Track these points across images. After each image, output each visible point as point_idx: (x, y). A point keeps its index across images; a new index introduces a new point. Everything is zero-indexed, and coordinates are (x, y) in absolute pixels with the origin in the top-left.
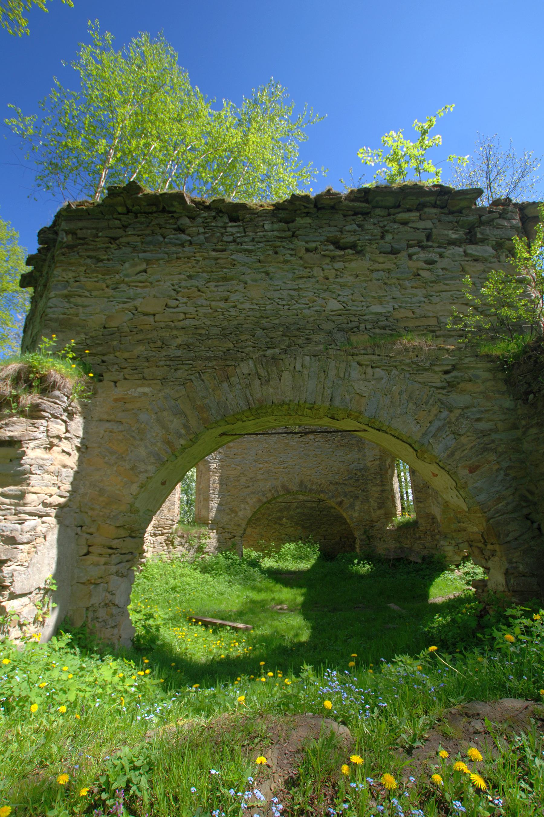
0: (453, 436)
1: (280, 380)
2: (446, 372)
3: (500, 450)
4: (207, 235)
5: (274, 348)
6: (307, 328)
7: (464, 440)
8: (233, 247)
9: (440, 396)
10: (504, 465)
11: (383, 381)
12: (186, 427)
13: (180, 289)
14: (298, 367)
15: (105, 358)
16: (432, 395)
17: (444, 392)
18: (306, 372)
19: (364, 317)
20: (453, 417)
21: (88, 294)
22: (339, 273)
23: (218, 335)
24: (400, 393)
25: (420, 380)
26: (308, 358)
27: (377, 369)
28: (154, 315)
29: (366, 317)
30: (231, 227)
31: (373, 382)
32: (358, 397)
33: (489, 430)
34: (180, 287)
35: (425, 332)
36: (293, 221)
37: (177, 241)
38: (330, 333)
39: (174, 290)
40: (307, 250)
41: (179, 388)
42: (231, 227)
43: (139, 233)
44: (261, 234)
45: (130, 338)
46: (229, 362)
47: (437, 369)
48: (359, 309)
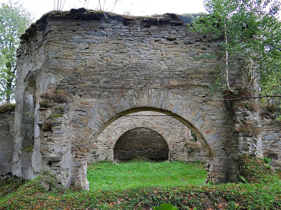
0: (203, 121)
1: (143, 98)
2: (203, 97)
3: (218, 126)
4: (113, 33)
5: (140, 84)
6: (154, 77)
7: (206, 122)
8: (124, 38)
9: (200, 106)
10: (219, 131)
11: (180, 100)
12: (109, 115)
13: (103, 57)
14: (150, 93)
15: (75, 86)
16: (197, 106)
17: (201, 104)
18: (152, 95)
19: (175, 73)
20: (204, 113)
21: (65, 57)
22: (167, 53)
23: (119, 78)
24: (186, 105)
25: (193, 100)
26: (153, 90)
27: (179, 95)
28: (94, 68)
29: (176, 73)
30: (124, 28)
31: (176, 100)
32: (171, 105)
33: (215, 119)
34: (103, 56)
35: (198, 80)
36: (150, 27)
37: (100, 34)
38: (162, 79)
39: (101, 57)
40: (156, 41)
41: (105, 99)
42: (124, 28)
43: (84, 29)
44: (136, 33)
45: (85, 78)
46: (124, 90)
47: (200, 95)
48: (174, 69)
